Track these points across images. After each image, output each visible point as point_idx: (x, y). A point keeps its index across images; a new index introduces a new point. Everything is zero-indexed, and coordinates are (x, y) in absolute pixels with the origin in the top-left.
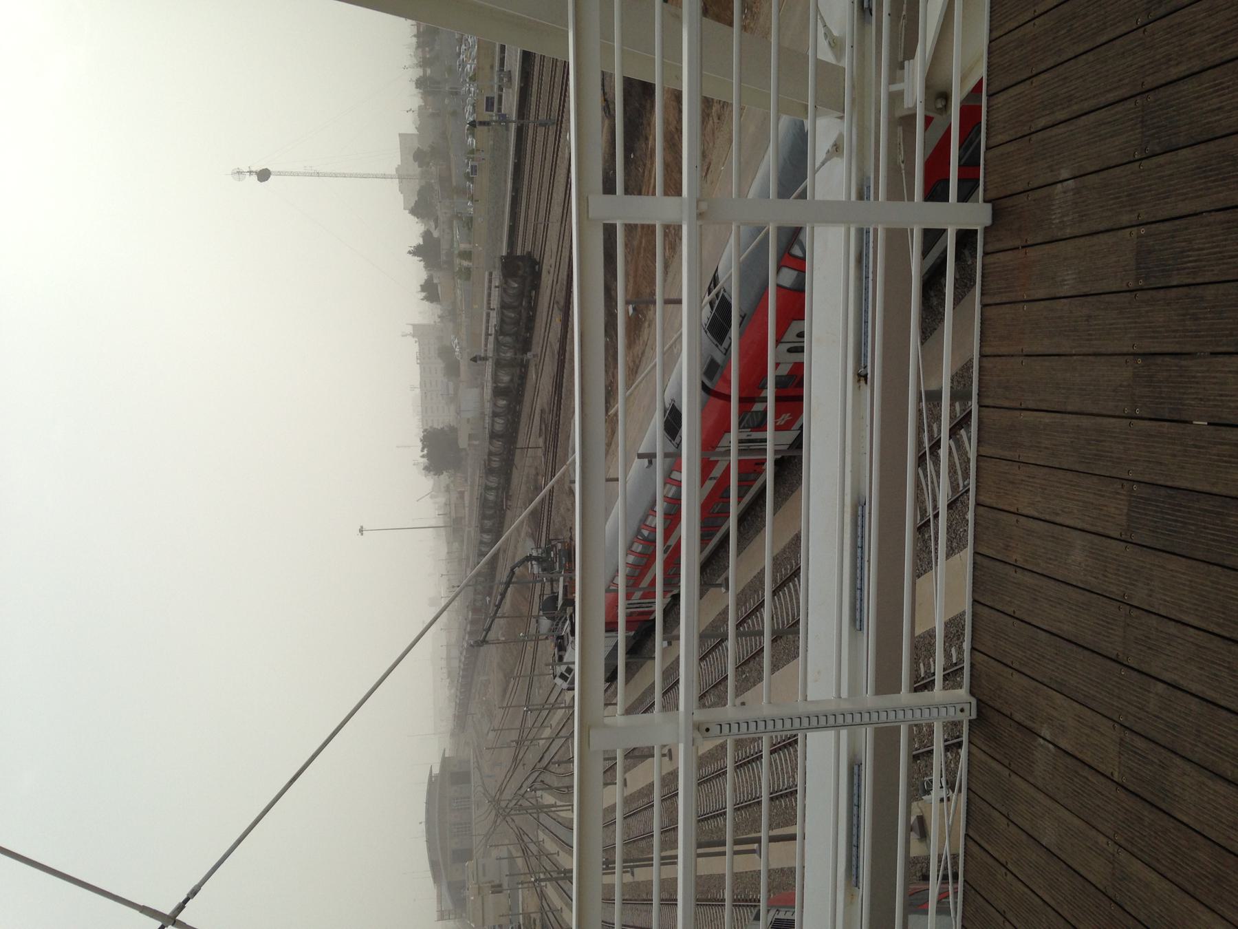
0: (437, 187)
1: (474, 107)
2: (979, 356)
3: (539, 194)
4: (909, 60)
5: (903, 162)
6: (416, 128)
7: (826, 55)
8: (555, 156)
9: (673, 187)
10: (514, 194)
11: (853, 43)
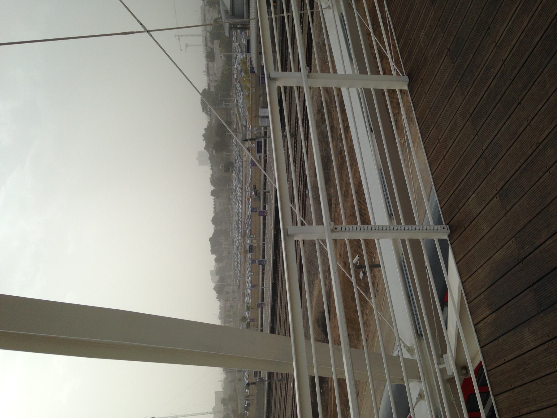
0: (231, 415)
1: (248, 376)
2: (480, 349)
3: (280, 412)
4: (444, 354)
5: (454, 400)
6: (223, 388)
7: (407, 355)
8: (286, 394)
9: (320, 222)
10: (268, 398)
11: (420, 359)
